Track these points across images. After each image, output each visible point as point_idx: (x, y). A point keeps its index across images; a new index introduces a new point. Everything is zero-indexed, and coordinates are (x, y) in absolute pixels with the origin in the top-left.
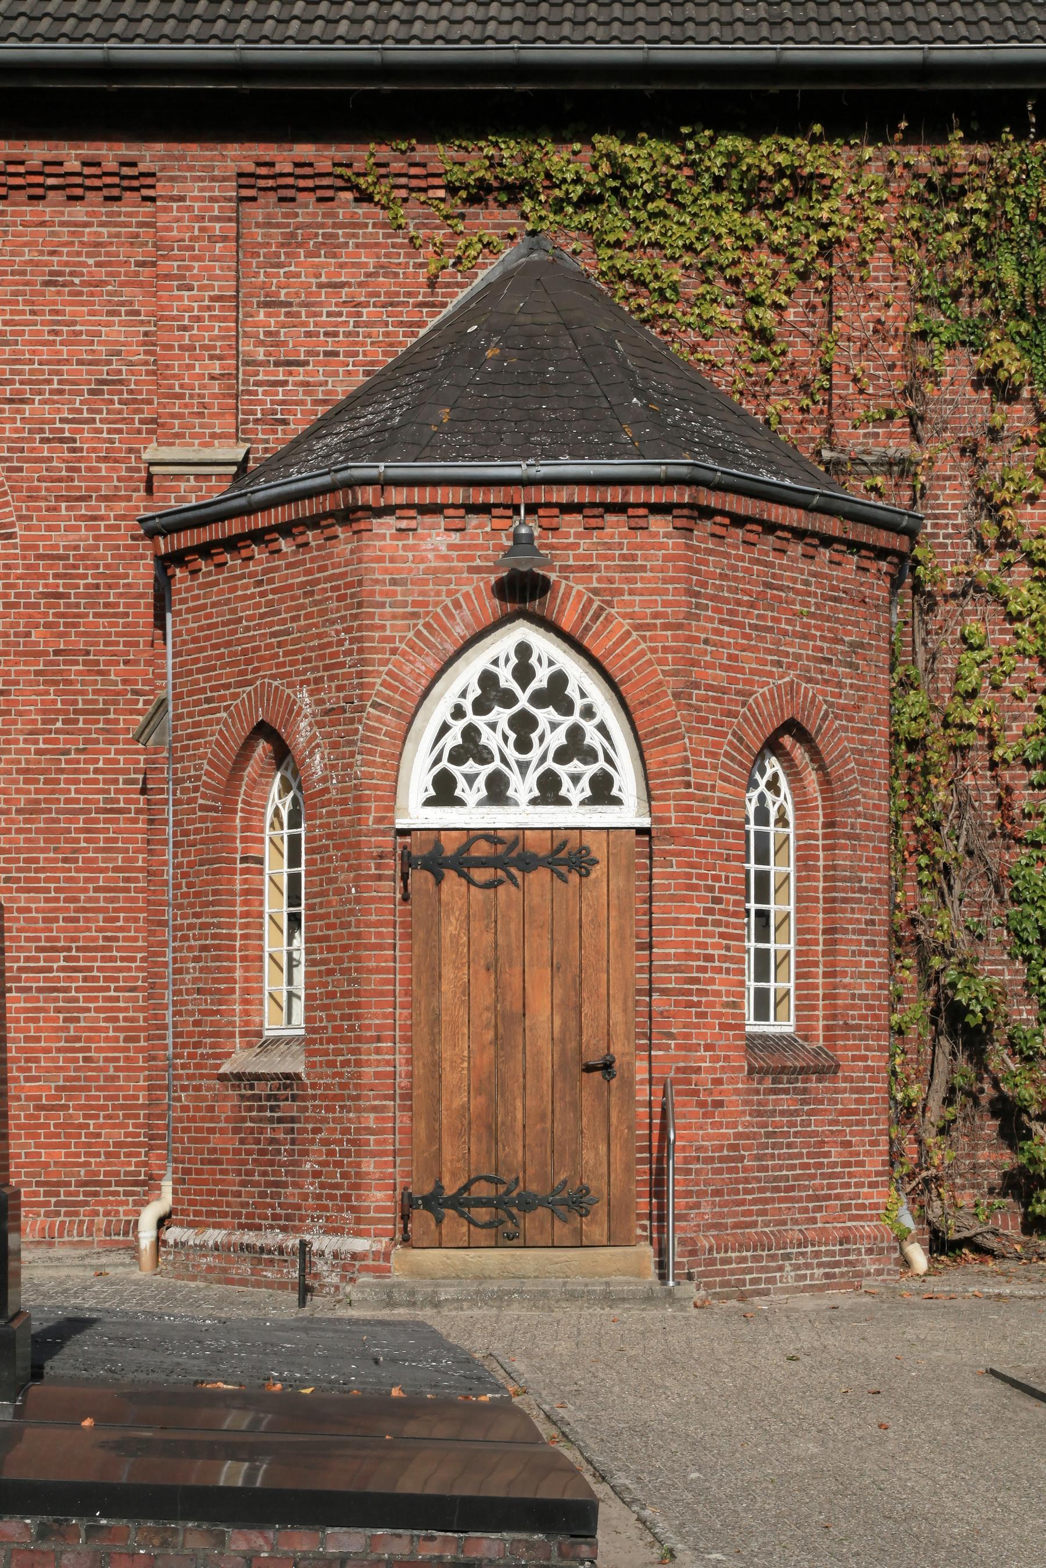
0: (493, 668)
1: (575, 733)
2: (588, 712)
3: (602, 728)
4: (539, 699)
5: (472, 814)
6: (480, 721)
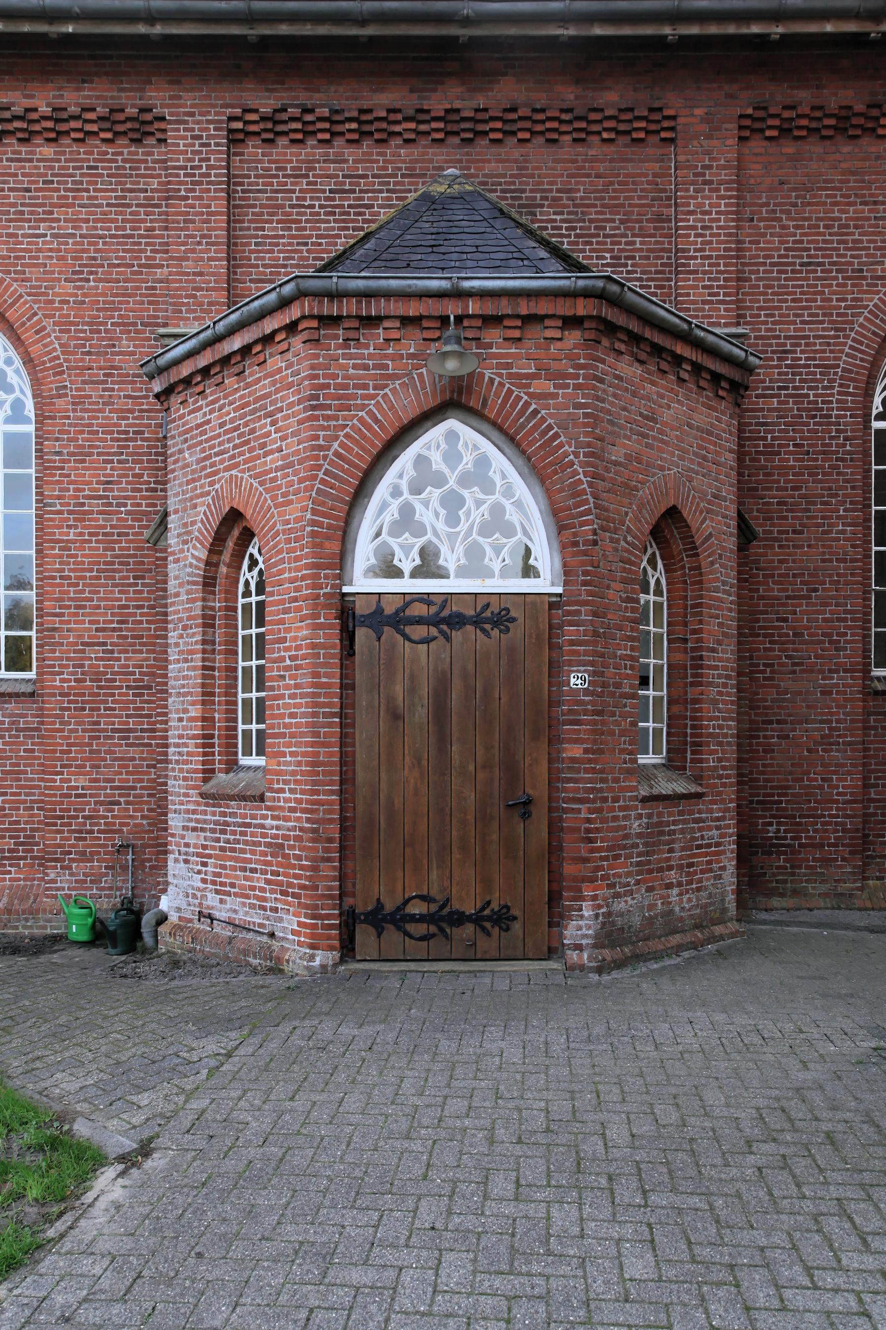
0: (425, 453)
1: (497, 511)
2: (508, 492)
3: (519, 505)
4: (465, 480)
6: (415, 502)
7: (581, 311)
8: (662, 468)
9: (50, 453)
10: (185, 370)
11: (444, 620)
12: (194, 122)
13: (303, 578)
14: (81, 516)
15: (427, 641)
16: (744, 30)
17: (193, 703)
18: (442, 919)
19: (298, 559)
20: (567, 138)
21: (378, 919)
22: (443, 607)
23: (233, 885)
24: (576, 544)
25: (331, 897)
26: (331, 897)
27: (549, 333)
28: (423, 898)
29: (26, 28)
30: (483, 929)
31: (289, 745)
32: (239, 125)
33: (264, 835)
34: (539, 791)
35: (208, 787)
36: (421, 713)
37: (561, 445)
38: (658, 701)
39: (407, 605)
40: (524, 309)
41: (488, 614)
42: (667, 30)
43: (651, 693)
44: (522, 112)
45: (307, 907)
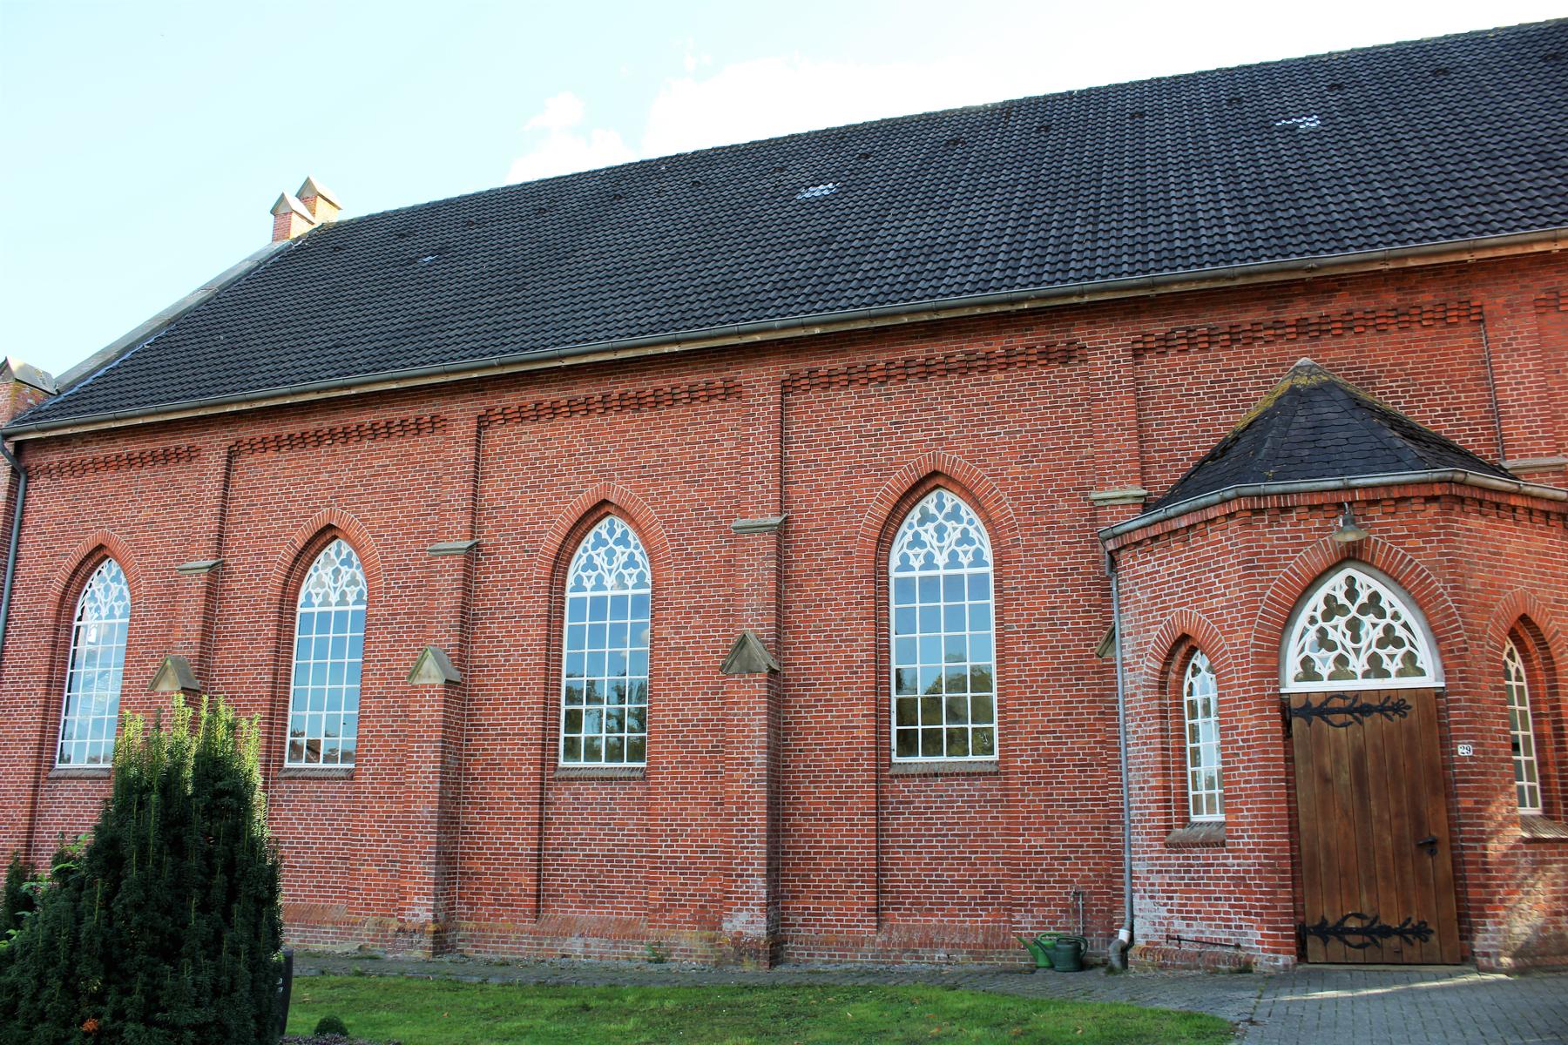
4: (1363, 610)
7: (1438, 492)
8: (1510, 588)
10: (1137, 537)
11: (1356, 710)
12: (1107, 350)
13: (1251, 684)
14: (1032, 633)
15: (1345, 725)
16: (1529, 250)
17: (1154, 776)
18: (1374, 932)
19: (1245, 670)
20: (1393, 328)
21: (1324, 931)
22: (1355, 700)
23: (1198, 912)
24: (1452, 651)
25: (1288, 914)
26: (1288, 914)
27: (1415, 507)
28: (1358, 916)
29: (996, 309)
30: (1407, 940)
31: (1246, 803)
32: (1140, 345)
33: (1226, 872)
34: (1440, 831)
35: (1168, 839)
36: (1345, 777)
37: (1432, 583)
38: (1529, 764)
39: (1328, 700)
40: (1396, 494)
41: (1389, 704)
42: (1466, 257)
43: (1522, 758)
44: (1356, 314)
45: (1269, 922)
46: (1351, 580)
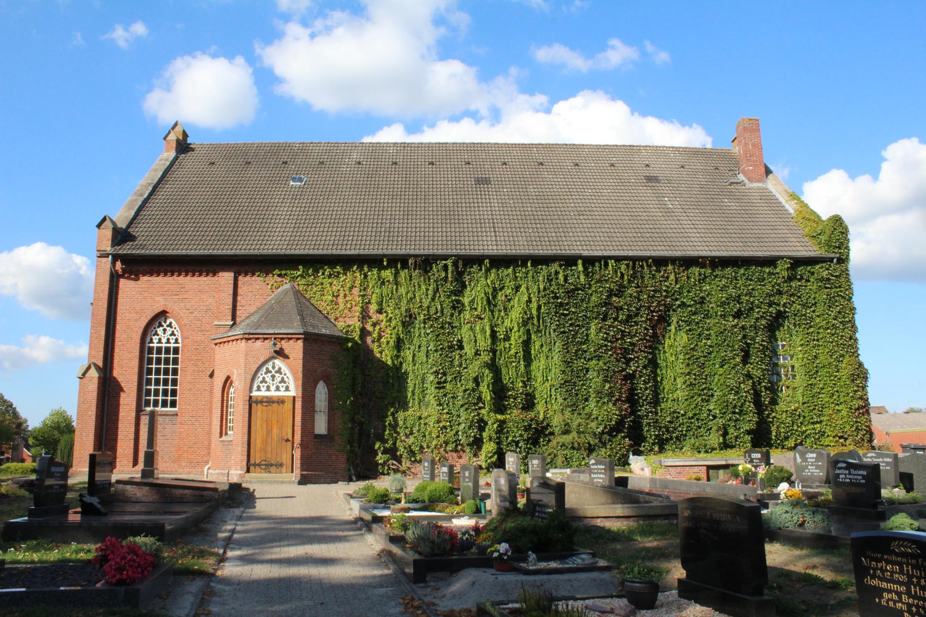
1: (283, 378)
5: (263, 393)
9: (576, 101)
46: (274, 363)
